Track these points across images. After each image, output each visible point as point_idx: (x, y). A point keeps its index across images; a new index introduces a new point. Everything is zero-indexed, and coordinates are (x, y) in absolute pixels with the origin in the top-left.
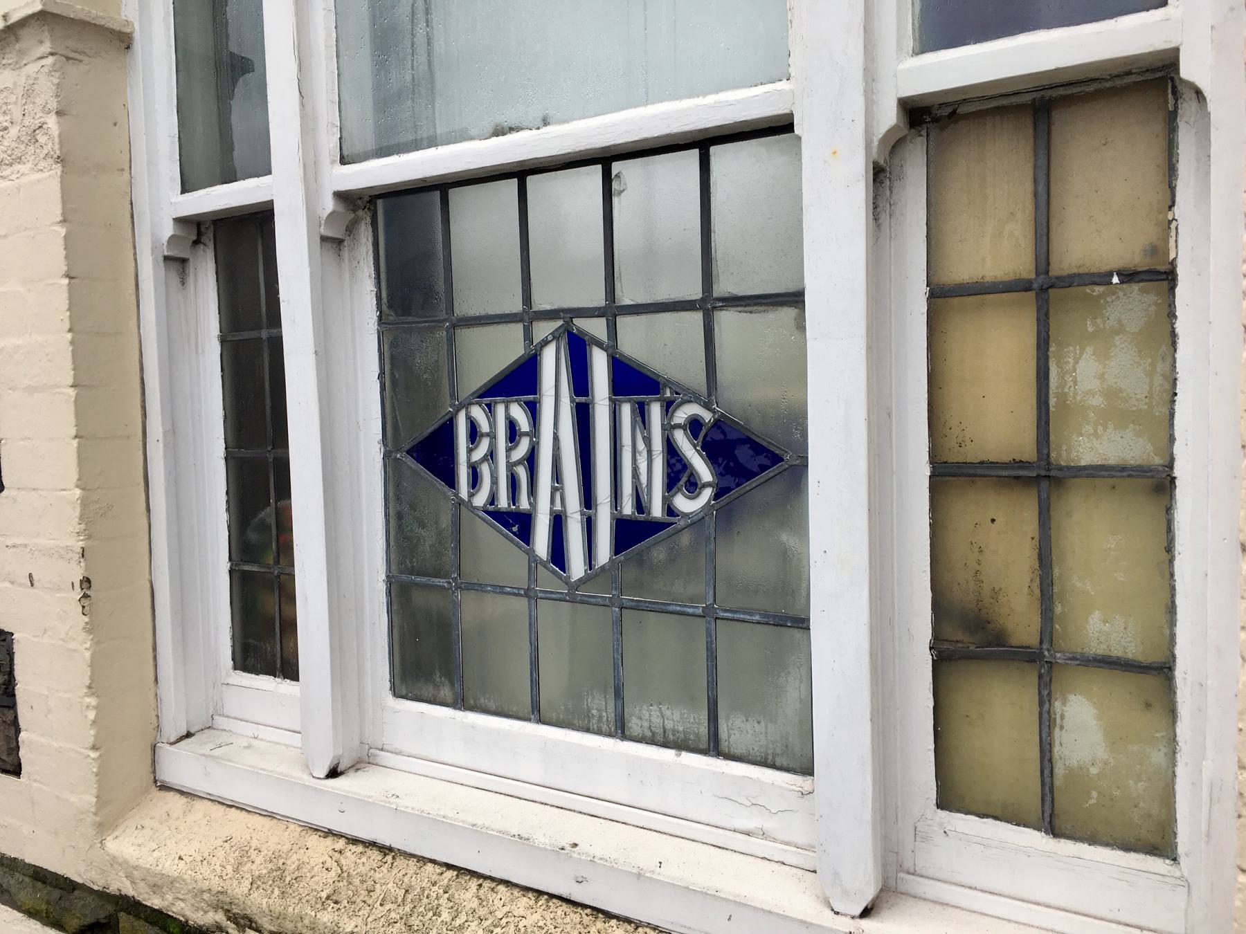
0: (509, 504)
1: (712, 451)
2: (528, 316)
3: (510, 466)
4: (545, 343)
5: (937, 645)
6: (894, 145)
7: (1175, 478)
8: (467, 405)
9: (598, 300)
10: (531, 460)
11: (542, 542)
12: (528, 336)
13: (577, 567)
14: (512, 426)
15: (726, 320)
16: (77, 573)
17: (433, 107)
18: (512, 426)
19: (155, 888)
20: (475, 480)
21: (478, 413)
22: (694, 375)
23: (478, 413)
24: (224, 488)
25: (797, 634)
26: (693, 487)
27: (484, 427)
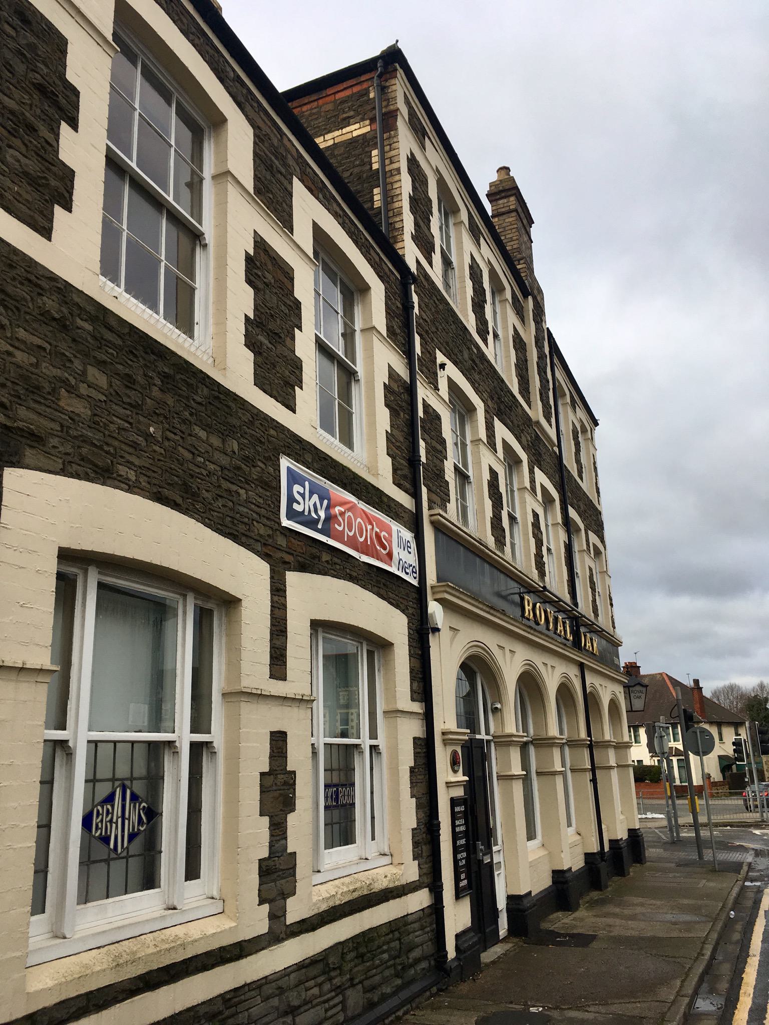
0: (687, 799)
2: (113, 780)
3: (106, 822)
4: (117, 787)
7: (701, 688)
8: (96, 806)
11: (112, 846)
12: (113, 786)
14: (108, 810)
18: (108, 810)
23: (99, 808)
24: (203, 827)
25: (326, 768)
27: (101, 812)
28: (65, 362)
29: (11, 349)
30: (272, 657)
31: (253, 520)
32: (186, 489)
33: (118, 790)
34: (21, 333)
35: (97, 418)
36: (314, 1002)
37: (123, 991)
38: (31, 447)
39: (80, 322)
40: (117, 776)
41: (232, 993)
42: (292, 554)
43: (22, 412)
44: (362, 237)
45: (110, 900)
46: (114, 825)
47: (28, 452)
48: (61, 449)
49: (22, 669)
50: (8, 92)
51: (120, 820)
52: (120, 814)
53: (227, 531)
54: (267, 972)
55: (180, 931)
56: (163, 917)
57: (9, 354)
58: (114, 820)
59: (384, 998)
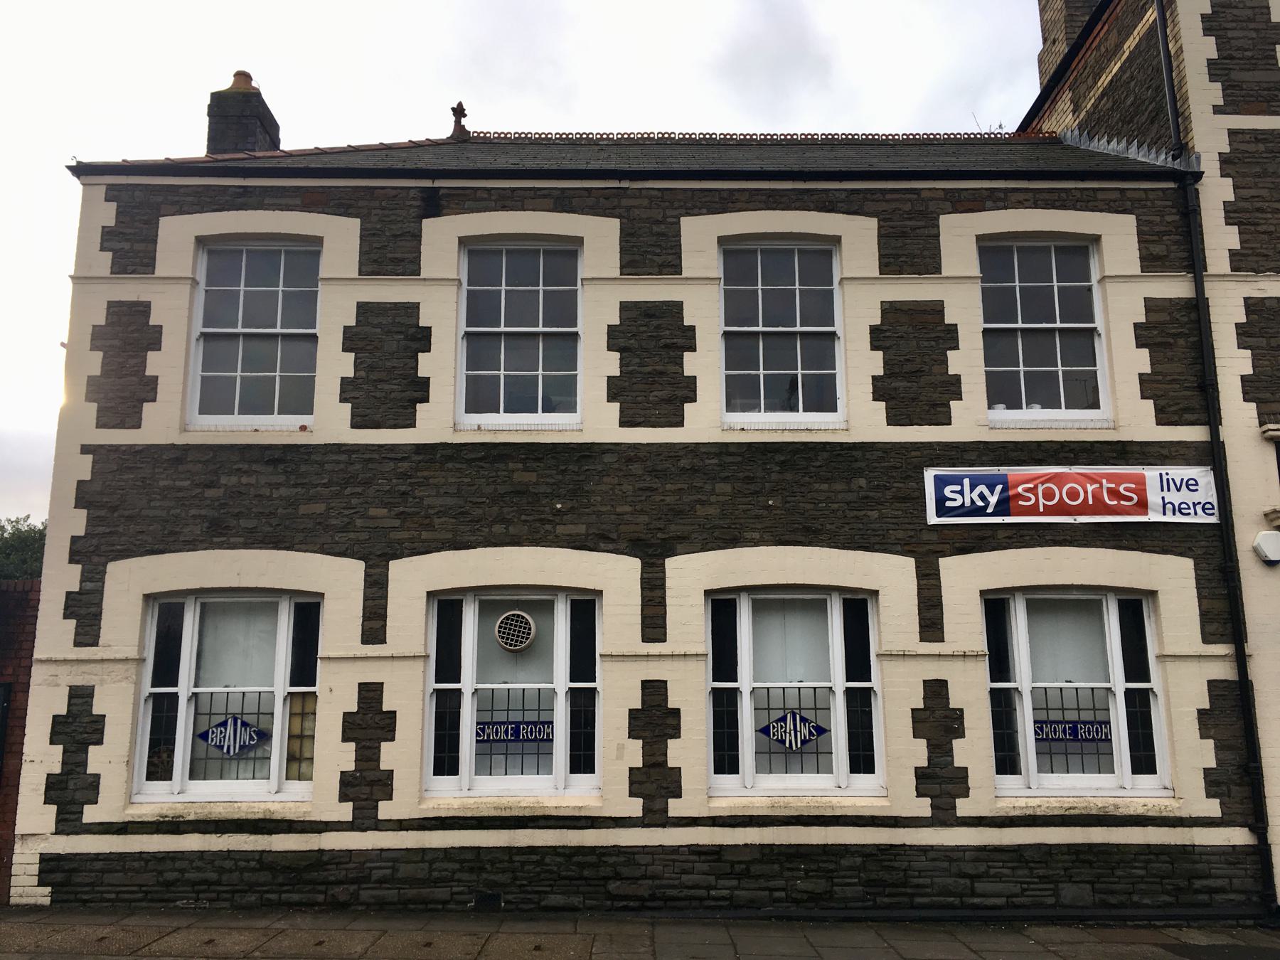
1: (257, 735)
5: (287, 759)
6: (191, 697)
9: (798, 707)
10: (224, 737)
11: (787, 745)
13: (232, 753)
14: (781, 726)
15: (261, 716)
16: (126, 760)
17: (119, 681)
18: (781, 726)
19: (139, 817)
20: (212, 740)
21: (214, 729)
22: (256, 724)
23: (214, 729)
26: (813, 736)
28: (699, 490)
29: (663, 498)
30: (921, 626)
31: (888, 530)
32: (807, 530)
33: (789, 715)
34: (668, 487)
35: (725, 512)
36: (1003, 879)
37: (778, 821)
38: (681, 543)
39: (708, 462)
40: (229, 712)
41: (642, 849)
42: (948, 543)
43: (673, 527)
44: (837, 194)
45: (788, 775)
46: (788, 735)
47: (679, 547)
48: (700, 538)
49: (685, 655)
50: (645, 364)
51: (792, 732)
52: (792, 728)
53: (857, 545)
54: (934, 843)
55: (834, 800)
56: (832, 790)
57: (663, 500)
58: (788, 731)
59: (1137, 905)
